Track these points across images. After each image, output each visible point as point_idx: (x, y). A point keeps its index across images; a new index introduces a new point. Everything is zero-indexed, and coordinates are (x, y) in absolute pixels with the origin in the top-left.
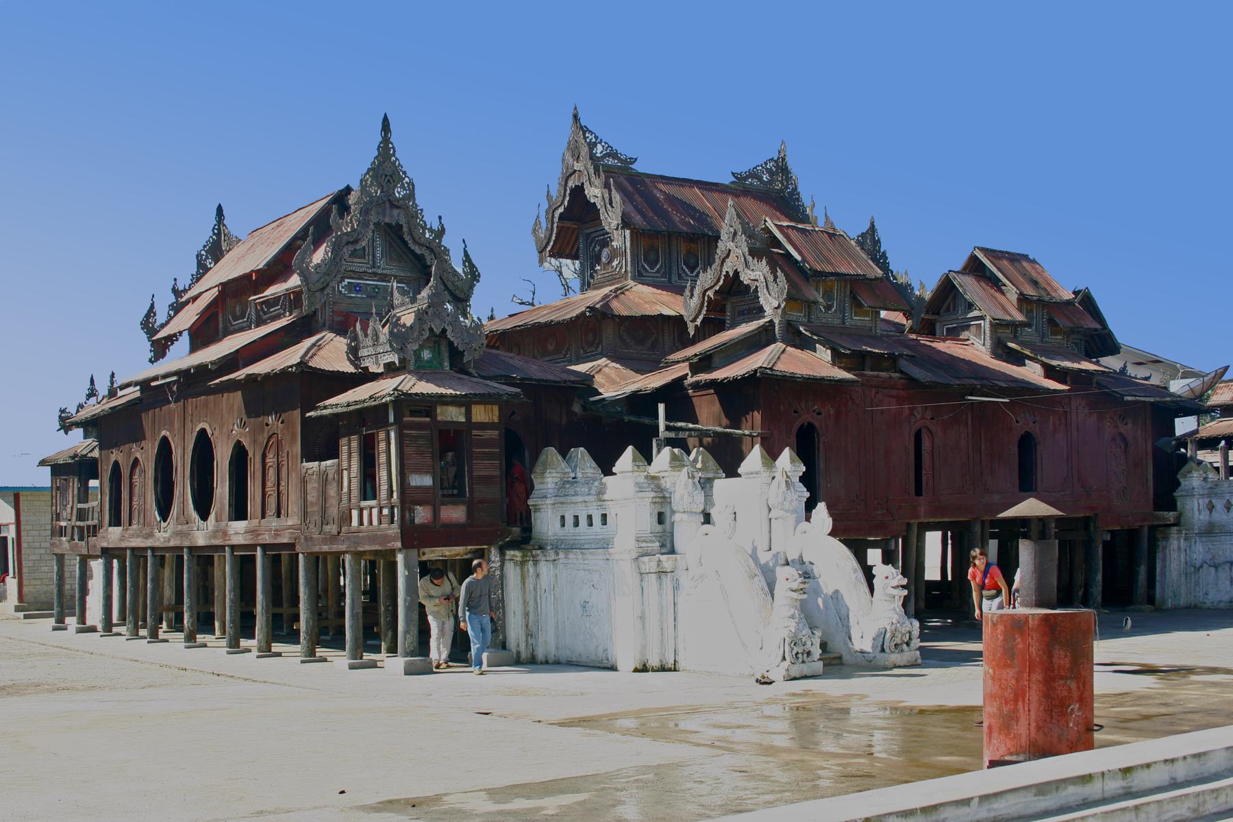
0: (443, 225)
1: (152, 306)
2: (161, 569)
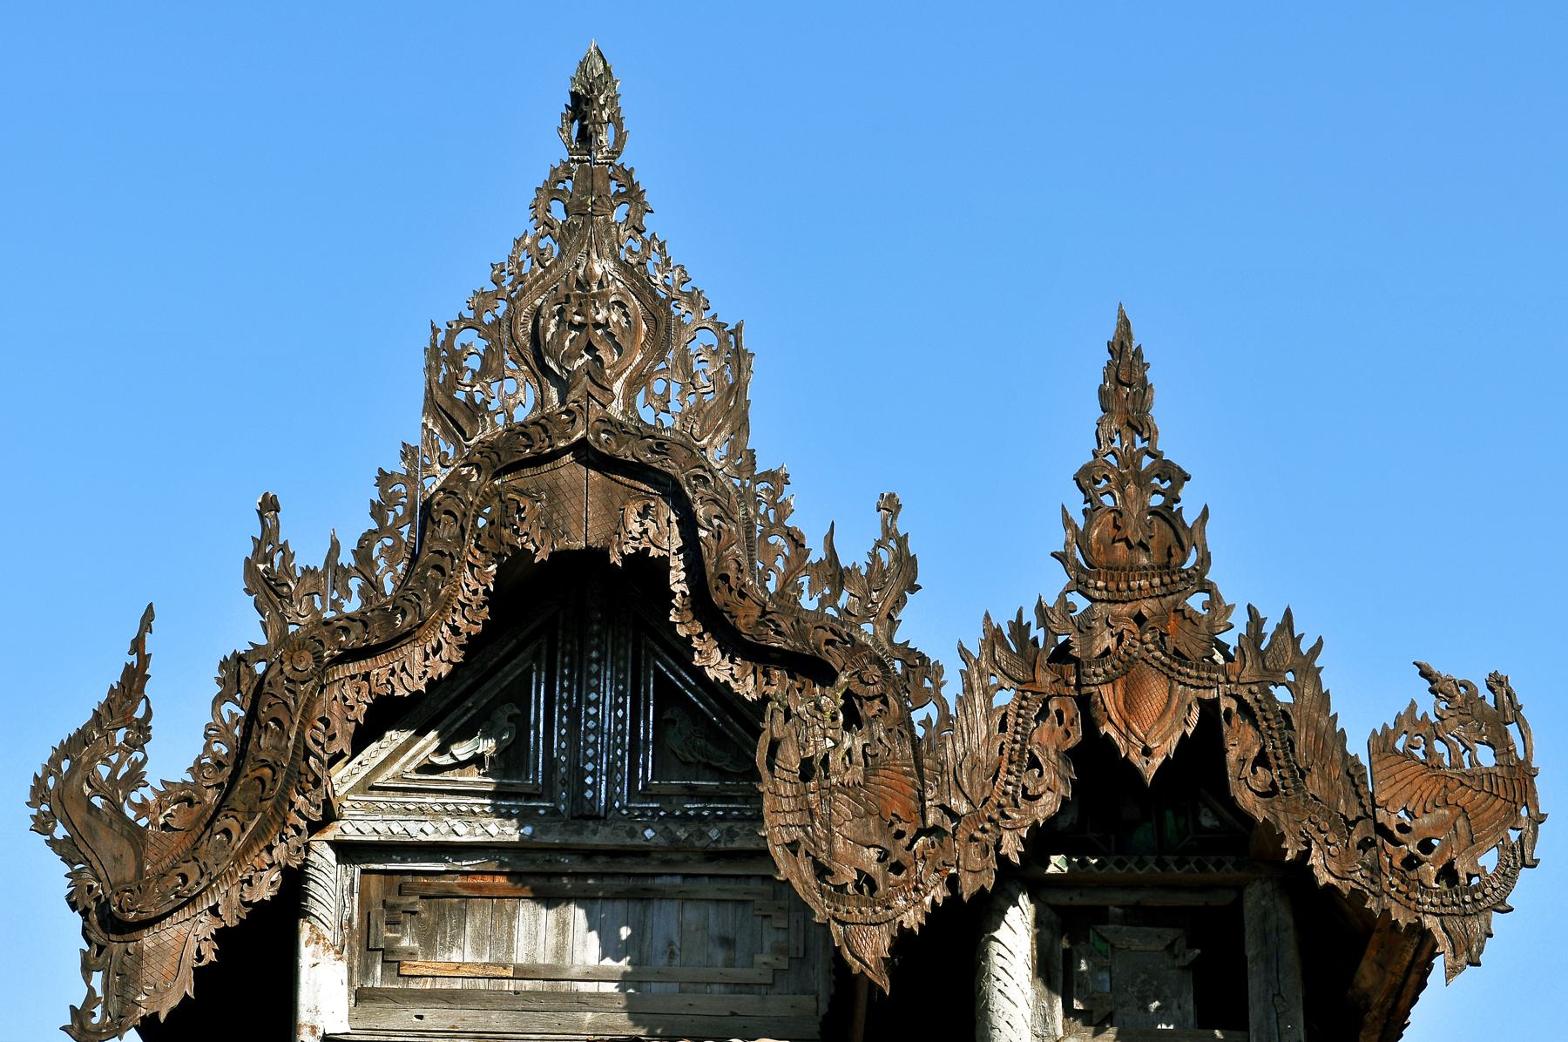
0: (902, 541)
1: (134, 680)
2: (698, 790)
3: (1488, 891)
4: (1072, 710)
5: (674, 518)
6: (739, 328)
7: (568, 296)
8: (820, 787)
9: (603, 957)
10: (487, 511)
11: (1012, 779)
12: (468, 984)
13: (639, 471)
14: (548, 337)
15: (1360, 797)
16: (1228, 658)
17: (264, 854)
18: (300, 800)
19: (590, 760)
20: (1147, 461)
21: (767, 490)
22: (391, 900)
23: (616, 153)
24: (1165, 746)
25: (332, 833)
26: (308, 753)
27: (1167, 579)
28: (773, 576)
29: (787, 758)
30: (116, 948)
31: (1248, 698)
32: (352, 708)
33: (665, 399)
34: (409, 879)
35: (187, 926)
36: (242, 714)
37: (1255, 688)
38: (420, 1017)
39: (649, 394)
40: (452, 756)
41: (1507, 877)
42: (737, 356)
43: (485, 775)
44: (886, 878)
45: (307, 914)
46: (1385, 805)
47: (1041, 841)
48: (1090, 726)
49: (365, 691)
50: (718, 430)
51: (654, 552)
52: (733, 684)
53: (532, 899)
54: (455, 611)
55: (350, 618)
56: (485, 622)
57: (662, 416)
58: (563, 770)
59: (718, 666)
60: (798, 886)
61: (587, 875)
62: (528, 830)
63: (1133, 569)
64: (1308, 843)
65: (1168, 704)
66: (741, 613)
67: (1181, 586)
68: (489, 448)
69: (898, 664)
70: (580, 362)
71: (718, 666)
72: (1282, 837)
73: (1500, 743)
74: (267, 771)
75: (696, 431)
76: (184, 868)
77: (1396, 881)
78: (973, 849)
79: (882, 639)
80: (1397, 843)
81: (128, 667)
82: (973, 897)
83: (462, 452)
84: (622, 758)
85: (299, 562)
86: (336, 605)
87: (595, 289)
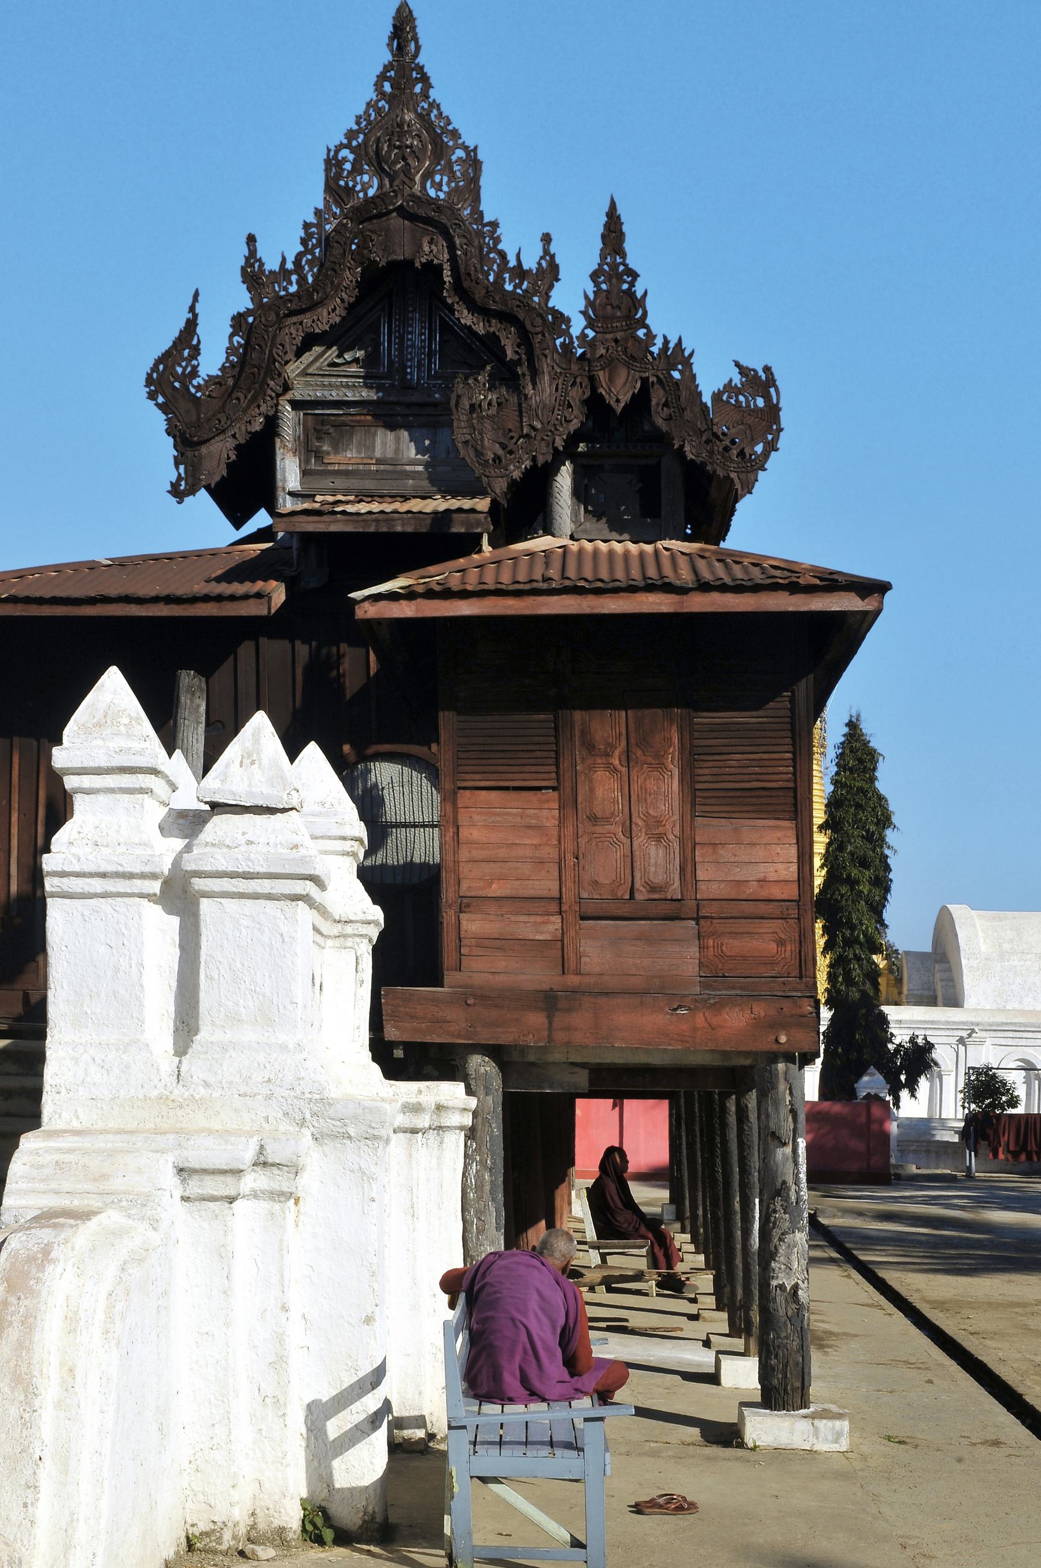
0: (553, 257)
1: (191, 325)
3: (758, 461)
4: (586, 382)
5: (445, 244)
6: (476, 148)
7: (393, 132)
8: (478, 417)
9: (417, 455)
10: (356, 241)
11: (560, 413)
12: (355, 467)
13: (428, 221)
14: (384, 153)
15: (707, 420)
16: (654, 358)
17: (256, 409)
18: (272, 383)
19: (409, 360)
20: (622, 268)
21: (489, 231)
22: (318, 427)
23: (416, 55)
24: (625, 398)
25: (289, 396)
26: (275, 360)
27: (628, 323)
28: (492, 273)
29: (464, 404)
30: (189, 454)
31: (661, 376)
32: (295, 338)
33: (440, 184)
34: (326, 417)
35: (220, 445)
36: (243, 342)
37: (664, 372)
38: (333, 483)
39: (433, 182)
40: (345, 359)
41: (766, 455)
42: (473, 163)
43: (360, 368)
44: (506, 457)
45: (279, 435)
46: (716, 424)
47: (573, 440)
48: (594, 389)
49: (300, 330)
50: (466, 200)
51: (436, 261)
52: (473, 327)
53: (384, 427)
54: (342, 291)
55: (292, 295)
56: (356, 296)
57: (439, 193)
58: (397, 365)
59: (466, 318)
60: (469, 461)
61: (407, 416)
62: (380, 394)
63: (614, 318)
64: (684, 441)
65: (627, 379)
66: (477, 292)
67: (634, 326)
68: (356, 210)
69: (550, 317)
70: (399, 166)
71: (466, 318)
72: (673, 438)
73: (767, 397)
74: (256, 370)
75: (455, 201)
76: (219, 416)
77: (720, 457)
78: (543, 444)
79: (543, 304)
80: (721, 441)
81: (188, 321)
82: (542, 465)
83: (343, 212)
84: (424, 359)
85: (268, 267)
86: (285, 289)
87: (406, 129)
